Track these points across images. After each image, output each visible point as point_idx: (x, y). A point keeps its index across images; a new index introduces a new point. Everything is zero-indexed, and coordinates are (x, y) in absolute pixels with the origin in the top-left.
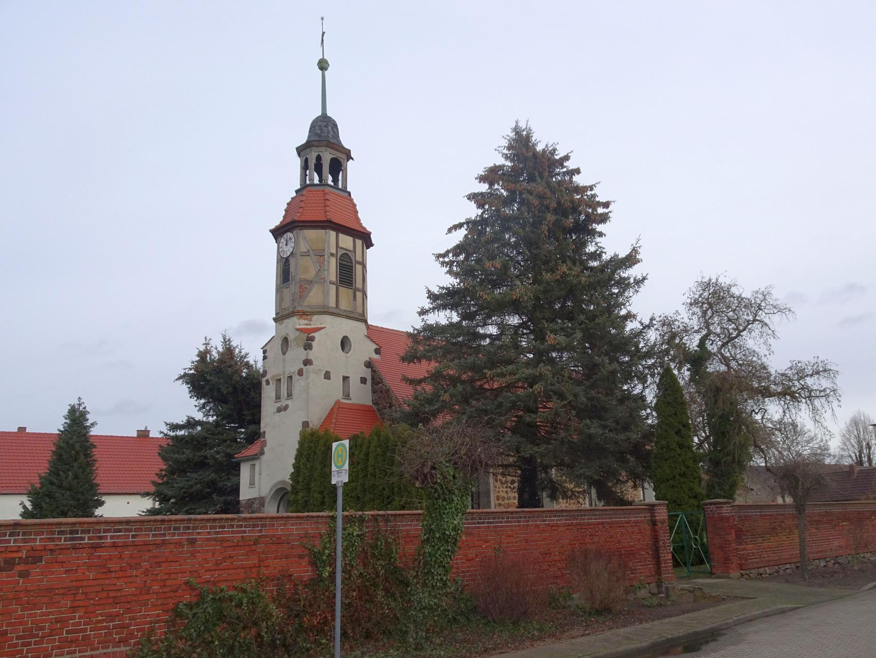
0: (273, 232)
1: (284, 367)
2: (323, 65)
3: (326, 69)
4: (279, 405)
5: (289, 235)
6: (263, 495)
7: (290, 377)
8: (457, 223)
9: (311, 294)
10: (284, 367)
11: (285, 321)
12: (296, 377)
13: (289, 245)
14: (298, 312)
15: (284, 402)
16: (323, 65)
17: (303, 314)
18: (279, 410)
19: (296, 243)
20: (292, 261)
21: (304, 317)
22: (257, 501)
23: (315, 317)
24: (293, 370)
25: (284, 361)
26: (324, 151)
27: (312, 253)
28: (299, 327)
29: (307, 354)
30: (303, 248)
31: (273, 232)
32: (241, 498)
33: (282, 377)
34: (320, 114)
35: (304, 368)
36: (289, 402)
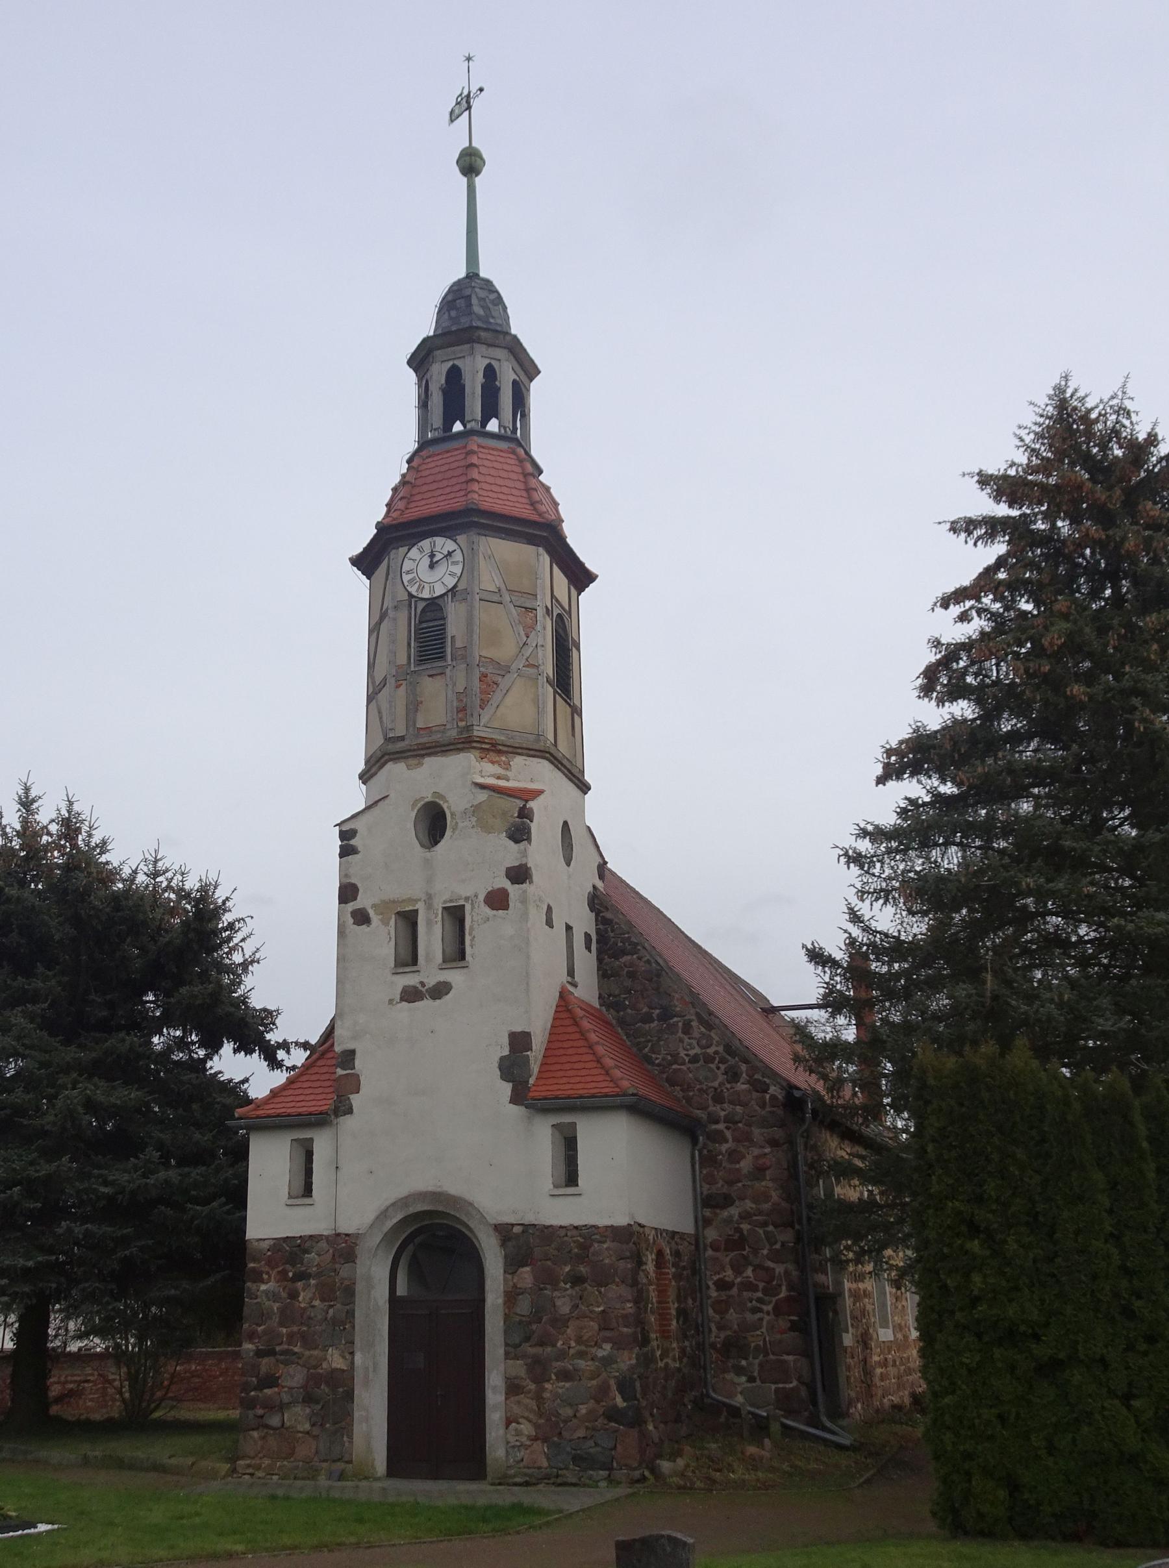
0: (357, 562)
1: (429, 880)
2: (470, 164)
3: (478, 173)
4: (411, 980)
5: (443, 545)
6: (348, 1225)
7: (456, 915)
8: (951, 589)
9: (509, 700)
10: (429, 880)
11: (427, 760)
12: (477, 915)
13: (441, 570)
14: (482, 740)
15: (429, 973)
16: (470, 164)
17: (493, 749)
18: (411, 995)
19: (469, 565)
20: (455, 615)
21: (493, 756)
22: (323, 1244)
23: (518, 761)
24: (465, 891)
25: (427, 863)
26: (471, 363)
27: (507, 598)
28: (481, 780)
29: (524, 853)
30: (489, 580)
31: (357, 562)
32: (253, 1231)
33: (420, 906)
34: (461, 273)
35: (513, 890)
36: (454, 977)
